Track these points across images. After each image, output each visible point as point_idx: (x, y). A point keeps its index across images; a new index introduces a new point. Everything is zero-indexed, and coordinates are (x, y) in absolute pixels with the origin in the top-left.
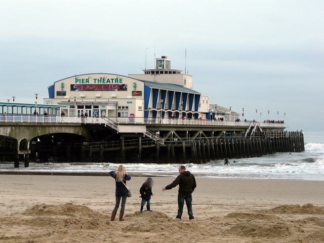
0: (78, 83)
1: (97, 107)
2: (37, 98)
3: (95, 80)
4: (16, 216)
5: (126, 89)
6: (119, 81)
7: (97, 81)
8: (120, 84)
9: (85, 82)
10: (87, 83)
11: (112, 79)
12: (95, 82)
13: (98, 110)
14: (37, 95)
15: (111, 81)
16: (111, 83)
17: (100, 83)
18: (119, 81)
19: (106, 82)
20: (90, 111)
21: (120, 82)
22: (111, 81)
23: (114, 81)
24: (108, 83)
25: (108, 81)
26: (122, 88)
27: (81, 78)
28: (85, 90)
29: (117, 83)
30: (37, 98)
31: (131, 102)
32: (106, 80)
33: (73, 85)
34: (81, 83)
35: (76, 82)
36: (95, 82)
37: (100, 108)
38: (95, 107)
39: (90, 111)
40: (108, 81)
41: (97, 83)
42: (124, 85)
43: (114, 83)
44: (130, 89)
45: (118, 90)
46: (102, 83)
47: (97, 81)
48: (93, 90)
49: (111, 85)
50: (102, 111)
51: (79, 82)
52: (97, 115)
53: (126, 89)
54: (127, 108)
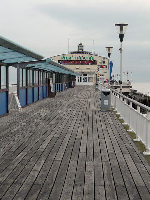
0: (63, 59)
1: (86, 75)
2: (121, 37)
3: (75, 57)
4: (19, 130)
5: (96, 64)
6: (91, 58)
7: (76, 58)
8: (92, 60)
9: (68, 58)
10: (70, 60)
11: (87, 57)
12: (75, 59)
13: (87, 77)
14: (121, 26)
15: (86, 58)
16: (86, 60)
17: (78, 60)
18: (91, 58)
19: (83, 59)
20: (81, 78)
21: (92, 59)
22: (86, 58)
23: (88, 58)
24: (84, 60)
25: (84, 58)
26: (94, 63)
27: (65, 56)
28: (68, 64)
29: (90, 60)
30: (121, 37)
31: (106, 72)
32: (83, 58)
33: (60, 61)
34: (66, 60)
35: (62, 58)
36: (75, 59)
37: (88, 76)
38: (84, 75)
39: (81, 78)
40: (84, 58)
41: (76, 60)
42: (95, 61)
43: (88, 60)
44: (99, 64)
45: (91, 64)
46: (80, 60)
47: (76, 58)
48: (74, 64)
49: (86, 61)
50: (89, 77)
51: (64, 58)
52: (86, 81)
53: (96, 64)
54: (103, 75)
